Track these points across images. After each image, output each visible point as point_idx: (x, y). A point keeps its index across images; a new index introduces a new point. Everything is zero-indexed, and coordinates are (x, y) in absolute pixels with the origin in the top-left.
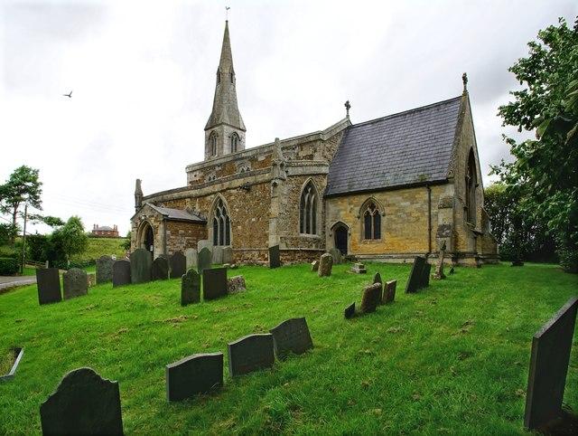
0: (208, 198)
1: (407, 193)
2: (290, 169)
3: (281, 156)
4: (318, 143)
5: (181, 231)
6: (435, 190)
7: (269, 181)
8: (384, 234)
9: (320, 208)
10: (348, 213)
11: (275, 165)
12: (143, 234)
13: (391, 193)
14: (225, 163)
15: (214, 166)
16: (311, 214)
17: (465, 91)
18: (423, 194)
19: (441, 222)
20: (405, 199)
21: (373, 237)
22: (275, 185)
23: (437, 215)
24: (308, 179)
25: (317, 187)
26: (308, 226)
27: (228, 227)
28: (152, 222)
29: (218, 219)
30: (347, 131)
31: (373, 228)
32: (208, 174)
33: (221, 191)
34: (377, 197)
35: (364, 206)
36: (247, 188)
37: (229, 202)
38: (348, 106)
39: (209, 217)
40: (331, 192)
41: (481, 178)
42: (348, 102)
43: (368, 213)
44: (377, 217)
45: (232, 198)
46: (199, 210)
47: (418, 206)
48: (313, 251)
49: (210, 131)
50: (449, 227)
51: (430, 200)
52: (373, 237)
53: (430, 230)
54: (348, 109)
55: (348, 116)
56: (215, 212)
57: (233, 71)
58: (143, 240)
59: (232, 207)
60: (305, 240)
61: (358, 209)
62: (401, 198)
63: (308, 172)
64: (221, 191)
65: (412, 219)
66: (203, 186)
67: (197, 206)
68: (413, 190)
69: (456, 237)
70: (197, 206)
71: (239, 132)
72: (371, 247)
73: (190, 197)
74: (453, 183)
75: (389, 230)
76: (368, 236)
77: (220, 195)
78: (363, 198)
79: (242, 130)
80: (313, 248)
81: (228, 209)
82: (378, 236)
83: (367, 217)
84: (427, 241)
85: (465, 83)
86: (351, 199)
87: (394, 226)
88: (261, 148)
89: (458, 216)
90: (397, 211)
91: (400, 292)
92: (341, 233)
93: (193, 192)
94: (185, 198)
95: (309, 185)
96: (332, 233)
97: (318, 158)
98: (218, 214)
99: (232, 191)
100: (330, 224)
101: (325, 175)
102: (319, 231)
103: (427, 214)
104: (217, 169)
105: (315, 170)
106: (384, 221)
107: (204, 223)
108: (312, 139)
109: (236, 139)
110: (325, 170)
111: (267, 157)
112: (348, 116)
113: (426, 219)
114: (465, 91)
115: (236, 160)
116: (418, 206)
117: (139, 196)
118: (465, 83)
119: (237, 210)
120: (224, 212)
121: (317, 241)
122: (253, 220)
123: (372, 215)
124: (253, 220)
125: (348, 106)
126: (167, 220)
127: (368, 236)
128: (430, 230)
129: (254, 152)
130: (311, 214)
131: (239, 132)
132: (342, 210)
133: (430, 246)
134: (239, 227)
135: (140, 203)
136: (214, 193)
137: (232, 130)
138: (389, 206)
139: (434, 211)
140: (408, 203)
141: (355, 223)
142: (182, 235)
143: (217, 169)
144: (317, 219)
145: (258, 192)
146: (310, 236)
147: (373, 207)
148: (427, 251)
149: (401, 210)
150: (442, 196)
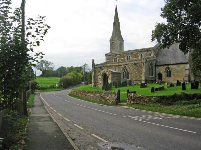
0: (121, 66)
1: (178, 65)
2: (147, 60)
7: (142, 63)
8: (172, 76)
9: (154, 69)
10: (162, 70)
11: (143, 59)
12: (103, 77)
15: (117, 55)
16: (152, 71)
20: (178, 67)
22: (143, 64)
24: (151, 61)
25: (153, 63)
26: (151, 74)
27: (128, 75)
28: (107, 73)
29: (127, 72)
31: (169, 74)
33: (126, 65)
34: (170, 66)
35: (166, 69)
36: (135, 64)
43: (167, 70)
49: (112, 42)
60: (151, 77)
63: (151, 60)
64: (126, 65)
68: (179, 65)
70: (117, 68)
71: (121, 42)
72: (169, 79)
73: (115, 66)
74: (189, 63)
75: (173, 75)
76: (168, 76)
77: (125, 65)
78: (166, 66)
80: (153, 80)
81: (128, 69)
82: (170, 76)
83: (167, 71)
87: (175, 74)
89: (190, 71)
90: (175, 70)
91: (175, 85)
92: (160, 75)
93: (106, 65)
94: (112, 66)
95: (151, 63)
96: (157, 75)
97: (152, 55)
99: (130, 65)
100: (157, 73)
101: (155, 60)
104: (118, 56)
105: (153, 59)
106: (172, 73)
108: (151, 49)
109: (121, 45)
110: (155, 58)
120: (127, 70)
121: (153, 78)
126: (113, 73)
127: (168, 76)
130: (152, 71)
134: (132, 74)
135: (94, 67)
136: (124, 65)
140: (178, 68)
141: (164, 73)
142: (116, 77)
143: (118, 56)
147: (169, 69)
149: (176, 69)
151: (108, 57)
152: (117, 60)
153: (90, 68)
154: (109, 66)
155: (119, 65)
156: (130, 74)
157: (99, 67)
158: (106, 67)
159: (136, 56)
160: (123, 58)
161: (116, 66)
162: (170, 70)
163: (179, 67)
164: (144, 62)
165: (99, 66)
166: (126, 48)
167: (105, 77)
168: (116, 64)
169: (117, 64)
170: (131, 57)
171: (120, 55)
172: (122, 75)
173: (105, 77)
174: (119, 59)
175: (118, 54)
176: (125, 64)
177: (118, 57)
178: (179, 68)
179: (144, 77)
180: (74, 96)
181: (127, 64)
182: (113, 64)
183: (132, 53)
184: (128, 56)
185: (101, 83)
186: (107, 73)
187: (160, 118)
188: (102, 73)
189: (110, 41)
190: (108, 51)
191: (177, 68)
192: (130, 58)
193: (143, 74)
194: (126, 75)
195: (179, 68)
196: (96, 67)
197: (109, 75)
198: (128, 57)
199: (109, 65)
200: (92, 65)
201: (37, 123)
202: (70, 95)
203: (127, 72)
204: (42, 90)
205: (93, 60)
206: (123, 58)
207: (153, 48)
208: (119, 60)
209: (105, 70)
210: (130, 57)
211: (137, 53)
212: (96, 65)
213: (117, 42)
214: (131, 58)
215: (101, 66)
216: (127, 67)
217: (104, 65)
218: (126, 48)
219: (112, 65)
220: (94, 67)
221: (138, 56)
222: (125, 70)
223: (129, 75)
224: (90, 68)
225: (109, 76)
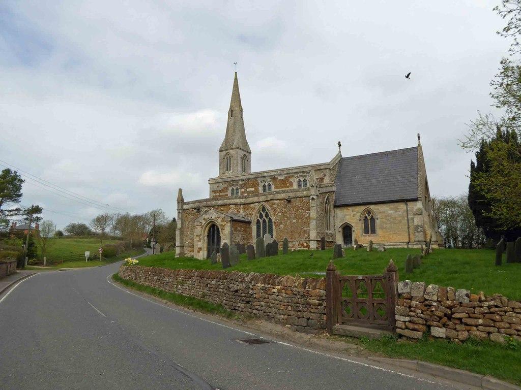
1: (392, 205)
3: (222, 166)
4: (328, 170)
5: (239, 228)
6: (410, 204)
8: (378, 230)
13: (382, 205)
14: (248, 179)
15: (238, 181)
17: (419, 144)
18: (402, 206)
19: (416, 223)
20: (392, 209)
21: (370, 232)
23: (413, 219)
27: (271, 227)
28: (219, 222)
29: (267, 220)
30: (341, 162)
32: (232, 186)
34: (372, 207)
35: (363, 213)
37: (272, 209)
38: (339, 145)
39: (254, 219)
40: (338, 203)
41: (273, 171)
42: (340, 142)
43: (366, 217)
44: (373, 219)
45: (275, 206)
46: (244, 214)
47: (400, 213)
48: (331, 242)
49: (224, 153)
50: (421, 227)
51: (407, 210)
52: (370, 232)
53: (409, 228)
54: (340, 147)
55: (340, 151)
56: (258, 215)
57: (242, 109)
58: (206, 234)
59: (275, 212)
61: (359, 214)
62: (388, 208)
65: (397, 222)
66: (226, 196)
67: (241, 211)
68: (396, 204)
69: (425, 232)
70: (241, 211)
71: (247, 154)
73: (236, 204)
75: (382, 228)
76: (366, 232)
77: (265, 204)
78: (363, 208)
79: (248, 152)
80: (331, 240)
81: (271, 213)
82: (373, 231)
83: (366, 219)
84: (407, 234)
85: (419, 139)
86: (354, 208)
88: (282, 170)
92: (347, 230)
93: (213, 203)
96: (341, 230)
98: (261, 216)
100: (339, 224)
101: (334, 192)
102: (332, 229)
103: (406, 218)
104: (240, 182)
106: (378, 222)
107: (249, 223)
108: (322, 167)
111: (286, 177)
112: (340, 151)
113: (406, 221)
114: (419, 144)
115: (259, 177)
116: (400, 213)
117: (181, 201)
118: (419, 139)
119: (280, 214)
120: (267, 215)
122: (294, 221)
123: (369, 218)
124: (294, 221)
125: (339, 145)
127: (366, 232)
128: (409, 228)
129: (275, 173)
131: (247, 154)
132: (347, 215)
133: (409, 237)
134: (282, 226)
135: (182, 207)
137: (243, 153)
138: (380, 212)
139: (410, 217)
141: (357, 223)
142: (240, 231)
143: (240, 182)
144: (331, 220)
145: (297, 203)
146: (328, 232)
147: (369, 213)
148: (407, 240)
149: (389, 215)
150: (415, 208)
151: (215, 186)
152: (237, 193)
153: (171, 213)
154: (221, 205)
155: (248, 202)
156: (277, 226)
157: (195, 208)
158: (213, 206)
159: (285, 183)
160: (252, 189)
161: (241, 205)
162: (372, 217)
163: (397, 210)
164: (313, 193)
165: (196, 205)
166: (256, 167)
167: (213, 232)
168: (238, 201)
169: (242, 201)
170: (273, 187)
171: (244, 180)
172: (254, 227)
173: (213, 232)
174: (243, 190)
175: (242, 178)
176: (262, 198)
177: (242, 187)
178: (396, 212)
179: (315, 231)
180: (126, 283)
181: (268, 201)
182: (232, 201)
183: (274, 178)
184: (267, 184)
185: (200, 249)
186: (219, 220)
187: (350, 328)
188: (204, 222)
189: (220, 151)
190: (215, 173)
191: (390, 212)
192: (269, 189)
193: (313, 224)
194: (266, 225)
195: (396, 212)
196: (185, 207)
197: (223, 227)
198: (264, 186)
199: (220, 202)
200: (178, 202)
201: (221, 245)
202: (116, 278)
203: (267, 220)
204: (46, 265)
205: (180, 190)
206: (252, 189)
207: (329, 164)
208: (242, 193)
209: (213, 214)
210: (269, 185)
211: (289, 177)
212: (188, 203)
213: (237, 154)
214: (273, 189)
215: (199, 207)
216: (267, 206)
217: (209, 203)
218: (256, 167)
219: (228, 202)
220: (182, 207)
221: (291, 185)
222: (264, 215)
223: (274, 227)
224: (171, 213)
225: (223, 229)
